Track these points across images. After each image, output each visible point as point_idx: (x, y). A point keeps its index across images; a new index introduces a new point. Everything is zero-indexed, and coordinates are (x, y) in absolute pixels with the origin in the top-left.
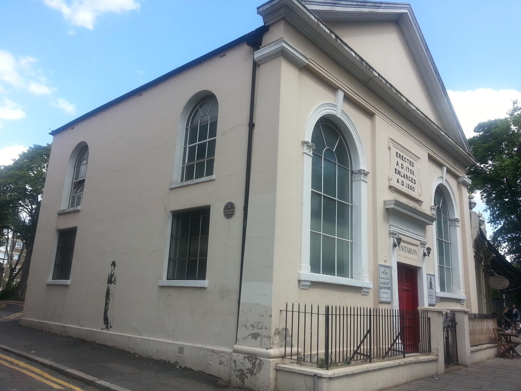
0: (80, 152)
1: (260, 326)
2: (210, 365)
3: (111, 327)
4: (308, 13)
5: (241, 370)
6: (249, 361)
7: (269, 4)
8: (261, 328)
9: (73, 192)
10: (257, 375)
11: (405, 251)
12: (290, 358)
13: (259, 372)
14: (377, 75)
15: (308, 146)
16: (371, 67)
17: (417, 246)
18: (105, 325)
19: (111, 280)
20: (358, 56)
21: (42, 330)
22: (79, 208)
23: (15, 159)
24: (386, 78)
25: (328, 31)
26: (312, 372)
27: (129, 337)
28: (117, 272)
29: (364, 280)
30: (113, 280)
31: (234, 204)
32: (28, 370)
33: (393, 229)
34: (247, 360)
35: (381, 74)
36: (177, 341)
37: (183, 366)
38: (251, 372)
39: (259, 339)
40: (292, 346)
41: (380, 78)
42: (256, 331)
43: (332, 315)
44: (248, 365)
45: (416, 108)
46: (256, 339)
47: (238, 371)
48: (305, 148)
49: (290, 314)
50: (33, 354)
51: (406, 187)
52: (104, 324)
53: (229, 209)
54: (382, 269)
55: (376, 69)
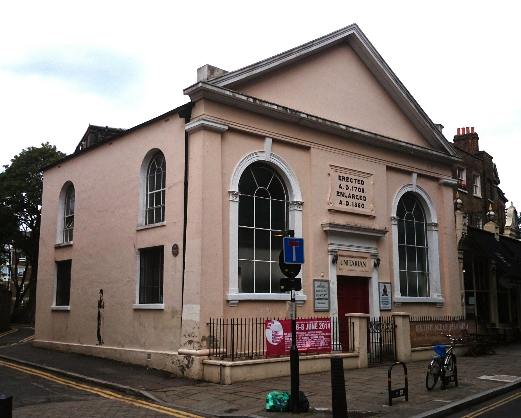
0: (68, 191)
1: (193, 335)
2: (167, 365)
3: (103, 343)
4: (223, 91)
5: (182, 366)
6: (187, 359)
7: (190, 89)
8: (193, 337)
9: (66, 226)
10: (191, 369)
11: (349, 264)
12: (215, 356)
13: (192, 366)
14: (305, 116)
15: (234, 194)
16: (296, 112)
17: (366, 258)
18: (99, 342)
19: (101, 305)
20: (280, 106)
21: (52, 349)
22: (71, 243)
23: (8, 165)
24: (315, 115)
25: (244, 98)
26: (219, 363)
27: (116, 350)
28: (105, 298)
29: (298, 294)
30: (102, 305)
31: (178, 245)
32: (42, 374)
33: (331, 247)
34: (185, 359)
35: (309, 113)
36: (147, 350)
37: (151, 367)
38: (188, 366)
39: (192, 344)
40: (220, 348)
41: (309, 117)
42: (191, 339)
43: (336, 322)
44: (186, 362)
45: (360, 130)
46: (191, 344)
47: (181, 366)
48: (231, 196)
49: (212, 325)
50: (45, 365)
51: (352, 206)
52: (98, 341)
53: (175, 249)
54: (317, 284)
55: (302, 111)
